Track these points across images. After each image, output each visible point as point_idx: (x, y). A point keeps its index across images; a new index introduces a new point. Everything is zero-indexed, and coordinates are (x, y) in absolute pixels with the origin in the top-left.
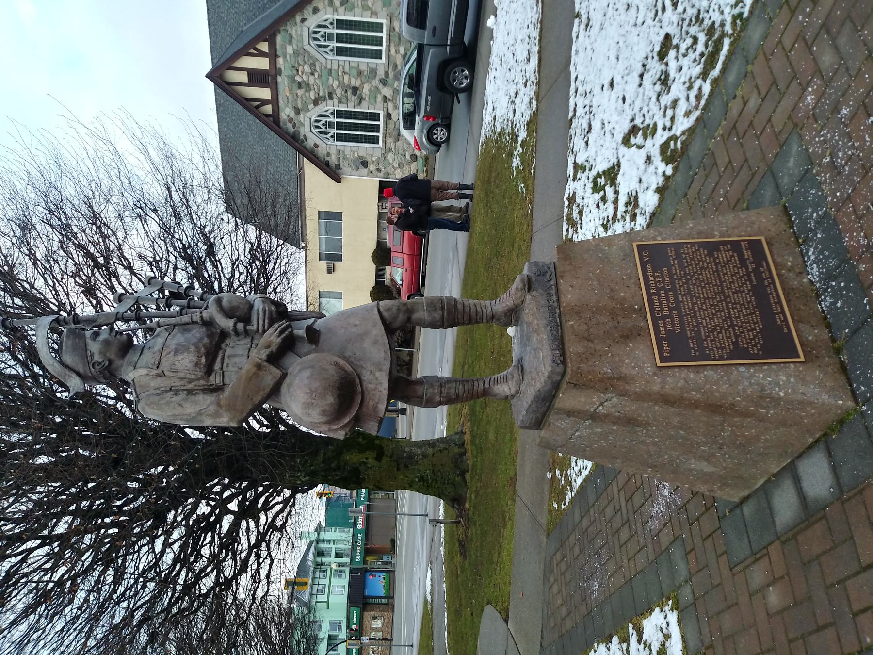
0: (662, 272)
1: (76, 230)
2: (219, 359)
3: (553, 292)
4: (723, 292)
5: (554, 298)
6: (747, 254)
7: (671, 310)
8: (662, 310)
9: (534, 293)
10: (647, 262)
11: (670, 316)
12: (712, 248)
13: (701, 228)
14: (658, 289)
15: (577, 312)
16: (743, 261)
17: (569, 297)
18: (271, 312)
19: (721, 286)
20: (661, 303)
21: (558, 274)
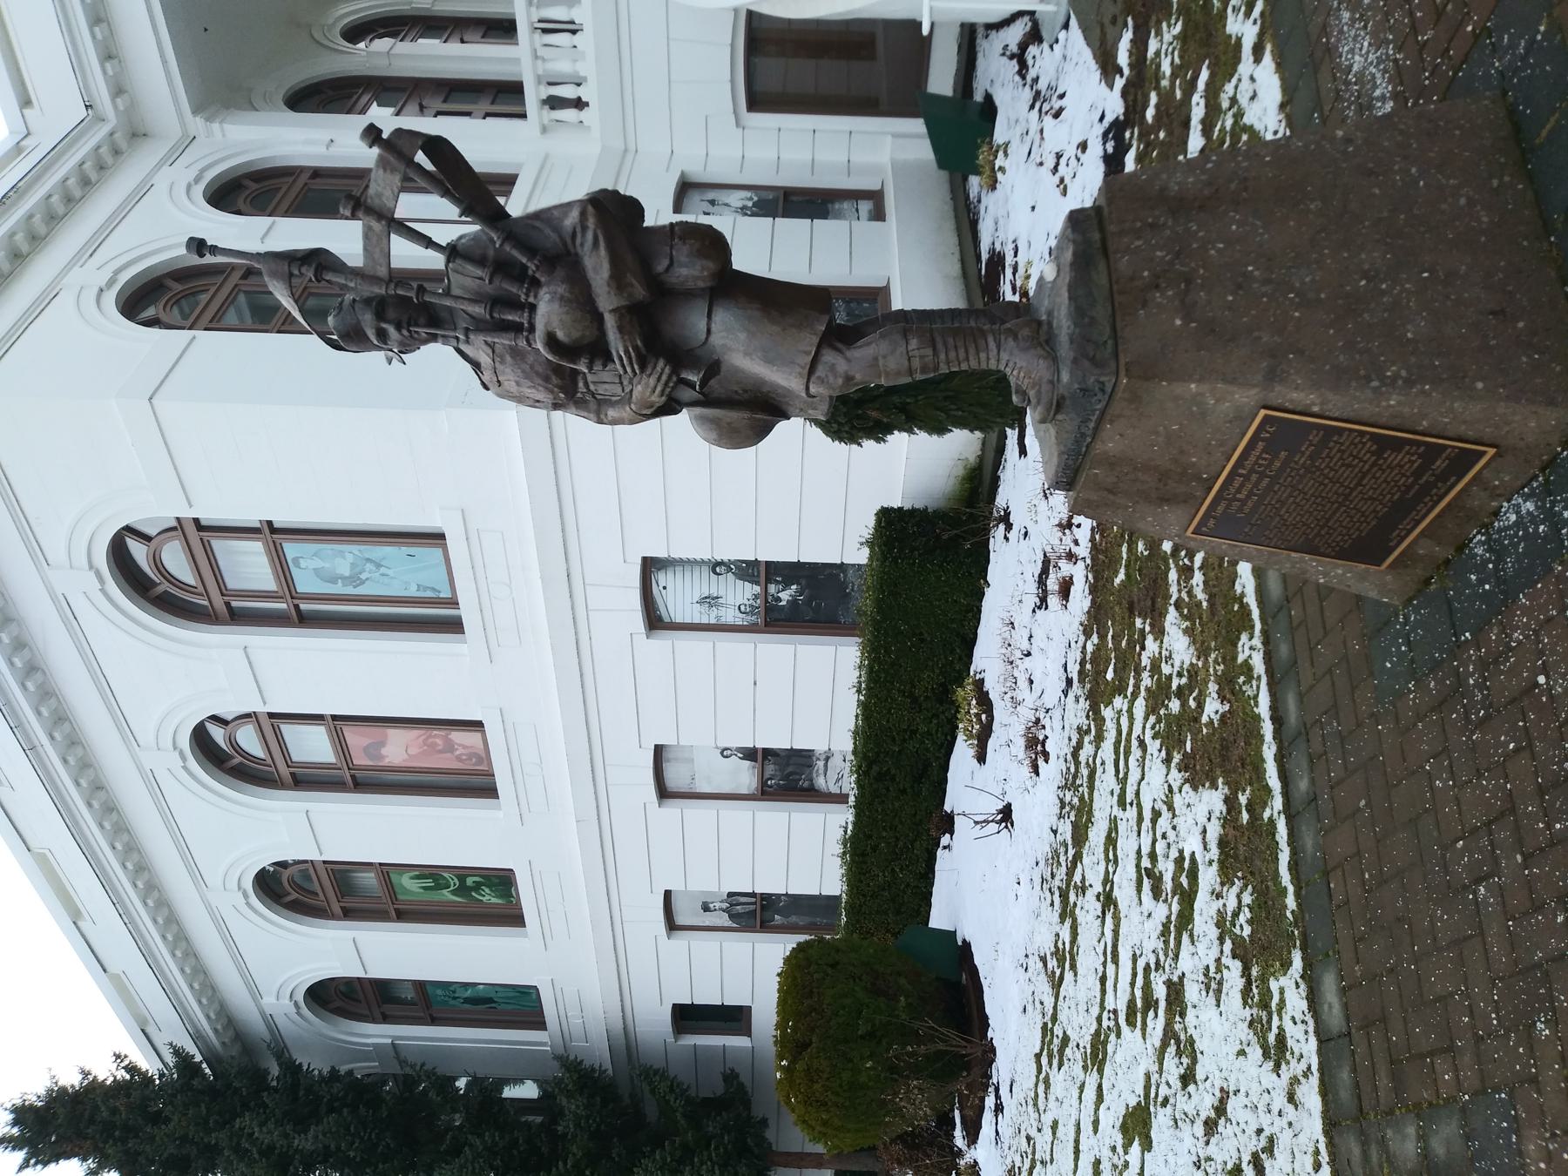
0: (1275, 456)
1: (1145, 661)
2: (581, 384)
3: (1094, 418)
4: (1347, 497)
5: (1092, 425)
6: (1440, 464)
7: (1251, 494)
8: (1239, 491)
9: (1059, 417)
10: (1263, 440)
11: (1244, 502)
12: (1383, 444)
13: (1406, 410)
14: (1252, 471)
15: (1111, 463)
16: (1418, 474)
17: (1111, 442)
18: (636, 348)
19: (1352, 490)
20: (1242, 485)
21: (1108, 417)
